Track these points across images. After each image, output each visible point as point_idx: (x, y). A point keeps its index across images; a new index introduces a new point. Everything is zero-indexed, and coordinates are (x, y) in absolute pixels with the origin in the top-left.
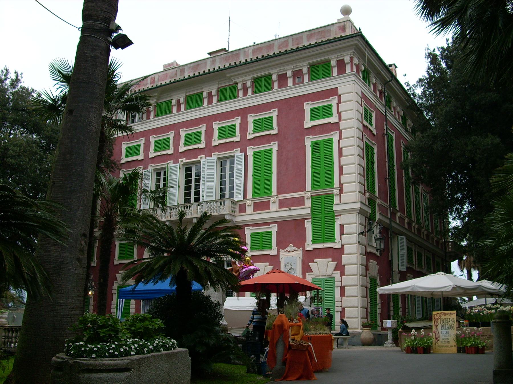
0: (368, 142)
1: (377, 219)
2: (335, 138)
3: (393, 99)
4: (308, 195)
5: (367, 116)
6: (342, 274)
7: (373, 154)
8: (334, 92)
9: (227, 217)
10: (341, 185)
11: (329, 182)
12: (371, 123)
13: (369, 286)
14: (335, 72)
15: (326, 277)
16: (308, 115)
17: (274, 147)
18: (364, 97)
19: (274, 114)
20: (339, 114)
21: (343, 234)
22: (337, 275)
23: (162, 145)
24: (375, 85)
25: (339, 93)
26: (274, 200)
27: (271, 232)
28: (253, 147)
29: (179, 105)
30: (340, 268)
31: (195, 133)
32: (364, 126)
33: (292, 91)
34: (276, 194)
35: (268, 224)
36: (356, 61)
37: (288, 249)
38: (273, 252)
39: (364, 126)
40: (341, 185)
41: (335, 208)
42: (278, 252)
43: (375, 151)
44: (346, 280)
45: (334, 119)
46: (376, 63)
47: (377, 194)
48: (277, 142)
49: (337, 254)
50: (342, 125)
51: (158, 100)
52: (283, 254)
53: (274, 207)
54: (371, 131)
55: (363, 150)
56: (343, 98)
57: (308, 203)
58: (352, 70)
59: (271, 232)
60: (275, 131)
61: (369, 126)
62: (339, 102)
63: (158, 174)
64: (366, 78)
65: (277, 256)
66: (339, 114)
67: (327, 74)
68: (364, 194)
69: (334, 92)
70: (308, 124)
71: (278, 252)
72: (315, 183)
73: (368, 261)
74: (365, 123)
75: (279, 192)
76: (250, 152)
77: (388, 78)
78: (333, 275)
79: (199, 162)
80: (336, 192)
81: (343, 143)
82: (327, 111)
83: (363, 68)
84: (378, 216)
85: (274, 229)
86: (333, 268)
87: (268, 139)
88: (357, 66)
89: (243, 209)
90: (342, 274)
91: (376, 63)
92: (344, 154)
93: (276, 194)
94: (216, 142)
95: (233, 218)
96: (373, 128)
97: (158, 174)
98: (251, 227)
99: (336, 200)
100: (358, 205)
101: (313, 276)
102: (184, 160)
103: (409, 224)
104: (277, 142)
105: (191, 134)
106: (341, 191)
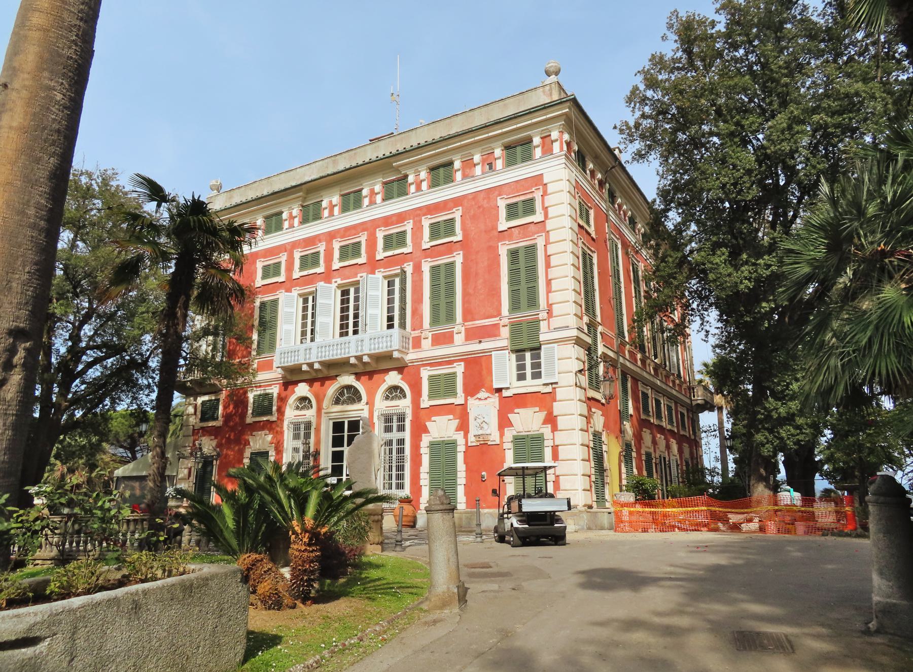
0: (586, 249)
1: (600, 353)
2: (540, 242)
3: (618, 194)
4: (505, 321)
5: (584, 213)
6: (555, 429)
7: (592, 264)
8: (538, 180)
9: (396, 355)
10: (550, 306)
11: (533, 302)
12: (588, 222)
13: (592, 445)
14: (538, 152)
15: (532, 433)
16: (503, 213)
17: (458, 259)
18: (577, 186)
19: (457, 214)
20: (545, 209)
21: (557, 430)
22: (547, 430)
23: (309, 261)
24: (593, 173)
25: (548, 229)
26: (459, 328)
27: (455, 373)
28: (429, 260)
29: (332, 207)
30: (551, 420)
31: (353, 244)
32: (579, 225)
33: (483, 182)
34: (524, 509)
35: (450, 363)
36: (566, 137)
37: (479, 396)
38: (459, 400)
39: (579, 225)
40: (550, 306)
41: (542, 338)
42: (466, 400)
43: (595, 261)
44: (560, 438)
45: (538, 217)
46: (595, 143)
47: (599, 319)
48: (461, 252)
49: (544, 400)
50: (549, 225)
51: (304, 201)
52: (471, 401)
53: (459, 339)
54: (589, 234)
55: (578, 258)
56: (553, 237)
57: (505, 332)
58: (561, 149)
59: (455, 373)
60: (459, 237)
61: (586, 226)
62: (545, 194)
63: (306, 301)
64: (581, 160)
65: (464, 406)
66: (545, 209)
67: (528, 157)
68: (581, 318)
69: (538, 180)
70: (503, 225)
71: (466, 400)
72: (515, 305)
73: (589, 410)
74: (582, 223)
75: (465, 320)
76: (426, 267)
77: (610, 163)
78: (542, 431)
79: (358, 282)
80: (543, 315)
81: (551, 249)
82: (529, 207)
83: (576, 148)
84: (601, 349)
85: (459, 369)
86: (542, 421)
87: (449, 248)
88: (569, 144)
89: (417, 343)
90: (555, 429)
91: (595, 143)
92: (554, 288)
93: (524, 509)
94: (380, 255)
95: (404, 356)
96: (592, 230)
97: (306, 301)
98: (428, 368)
99: (543, 325)
100: (575, 333)
101: (515, 433)
102: (339, 281)
103: (643, 361)
104: (461, 252)
105: (347, 245)
106: (550, 313)
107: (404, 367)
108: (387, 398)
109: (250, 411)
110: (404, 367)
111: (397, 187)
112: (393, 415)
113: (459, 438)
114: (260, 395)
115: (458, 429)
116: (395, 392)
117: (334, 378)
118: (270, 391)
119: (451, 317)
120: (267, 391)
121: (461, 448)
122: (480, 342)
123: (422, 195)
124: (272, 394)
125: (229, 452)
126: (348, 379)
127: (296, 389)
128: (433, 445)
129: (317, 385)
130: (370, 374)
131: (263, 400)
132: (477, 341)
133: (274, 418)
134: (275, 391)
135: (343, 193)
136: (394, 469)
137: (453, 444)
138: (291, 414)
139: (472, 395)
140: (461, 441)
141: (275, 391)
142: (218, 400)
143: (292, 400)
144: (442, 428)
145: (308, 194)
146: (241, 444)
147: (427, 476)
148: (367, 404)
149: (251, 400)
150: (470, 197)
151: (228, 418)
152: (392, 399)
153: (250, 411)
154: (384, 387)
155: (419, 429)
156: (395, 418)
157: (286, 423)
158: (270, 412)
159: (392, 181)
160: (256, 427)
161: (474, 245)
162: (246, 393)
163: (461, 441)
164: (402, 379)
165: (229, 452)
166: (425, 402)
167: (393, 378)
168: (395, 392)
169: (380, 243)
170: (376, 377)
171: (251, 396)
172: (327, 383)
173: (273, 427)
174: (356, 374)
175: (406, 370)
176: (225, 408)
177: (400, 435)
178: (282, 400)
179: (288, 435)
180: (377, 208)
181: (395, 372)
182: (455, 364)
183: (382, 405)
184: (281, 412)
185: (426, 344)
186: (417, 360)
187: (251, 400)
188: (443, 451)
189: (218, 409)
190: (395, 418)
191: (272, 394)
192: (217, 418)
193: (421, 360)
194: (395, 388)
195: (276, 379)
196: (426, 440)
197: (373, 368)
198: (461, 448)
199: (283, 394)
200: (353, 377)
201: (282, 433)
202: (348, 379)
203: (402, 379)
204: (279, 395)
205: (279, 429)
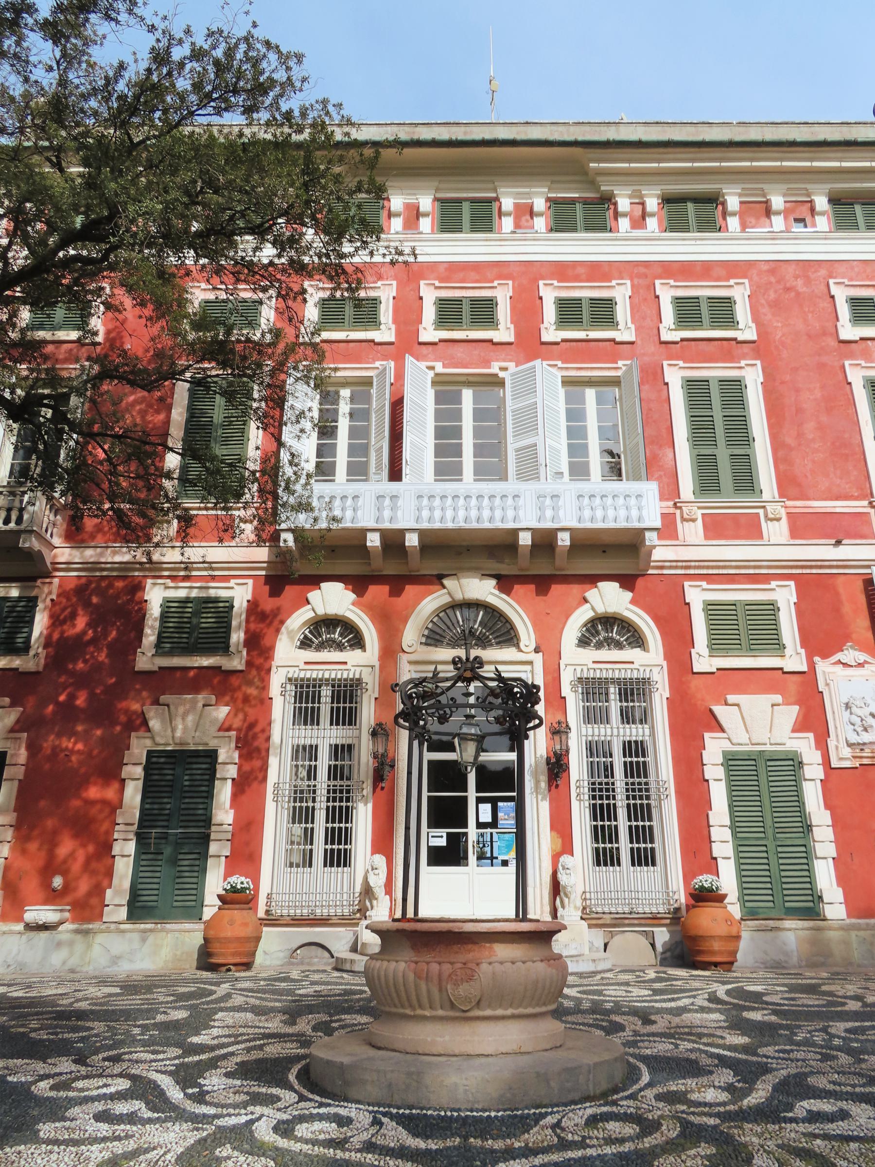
35: (766, 578)
37: (839, 656)
38: (794, 660)
52: (823, 666)
65: (809, 677)
85: (785, 596)
98: (704, 584)
101: (727, 746)
102: (439, 368)
105: (459, 301)
107: (636, 576)
108: (305, 644)
109: (150, 637)
110: (636, 576)
111: (592, 211)
112: (607, 681)
113: (804, 746)
114: (187, 600)
115: (800, 727)
116: (607, 629)
117: (438, 579)
118: (223, 594)
119: (746, 481)
120: (212, 593)
121: (814, 771)
122: (838, 543)
123: (640, 239)
124: (230, 602)
125: (67, 743)
126: (481, 588)
127: (314, 596)
128: (730, 760)
129: (377, 592)
130: (543, 584)
131: (196, 613)
132: (833, 541)
133: (237, 663)
134: (240, 594)
135: (439, 195)
136: (320, 816)
137: (795, 763)
138: (289, 658)
139: (825, 656)
140: (811, 757)
141: (240, 594)
142: (31, 603)
143: (297, 621)
144: (757, 722)
145: (579, 174)
146: (113, 723)
147: (727, 834)
148: (537, 650)
149: (155, 609)
150: (765, 267)
151: (61, 650)
152: (320, 647)
153: (150, 637)
154: (582, 616)
155: (693, 722)
156: (326, 692)
157: (277, 680)
158: (222, 646)
159: (573, 201)
160: (164, 684)
161: (785, 354)
162: (138, 587)
163: (811, 757)
164: (633, 602)
165: (67, 743)
166: (704, 660)
167: (609, 597)
168: (607, 629)
169: (429, 313)
170: (557, 590)
171: (156, 596)
172: (410, 590)
173: (242, 687)
174: (498, 577)
175: (640, 582)
176: (56, 621)
177: (599, 732)
178: (264, 622)
179: (281, 709)
180: (525, 238)
181: (339, 586)
182: (774, 584)
183: (578, 660)
184: (260, 648)
185: (692, 530)
186: (675, 564)
187: (155, 609)
188: (763, 779)
189: (31, 622)
190: (613, 690)
191: (230, 602)
192: (26, 648)
193: (687, 564)
194: (608, 621)
195: (250, 565)
196: (714, 748)
197: (541, 565)
198: (814, 771)
199: (269, 604)
200: (490, 584)
201: (265, 702)
202: (481, 588)
203: (633, 602)
204: (253, 607)
205: (252, 691)
